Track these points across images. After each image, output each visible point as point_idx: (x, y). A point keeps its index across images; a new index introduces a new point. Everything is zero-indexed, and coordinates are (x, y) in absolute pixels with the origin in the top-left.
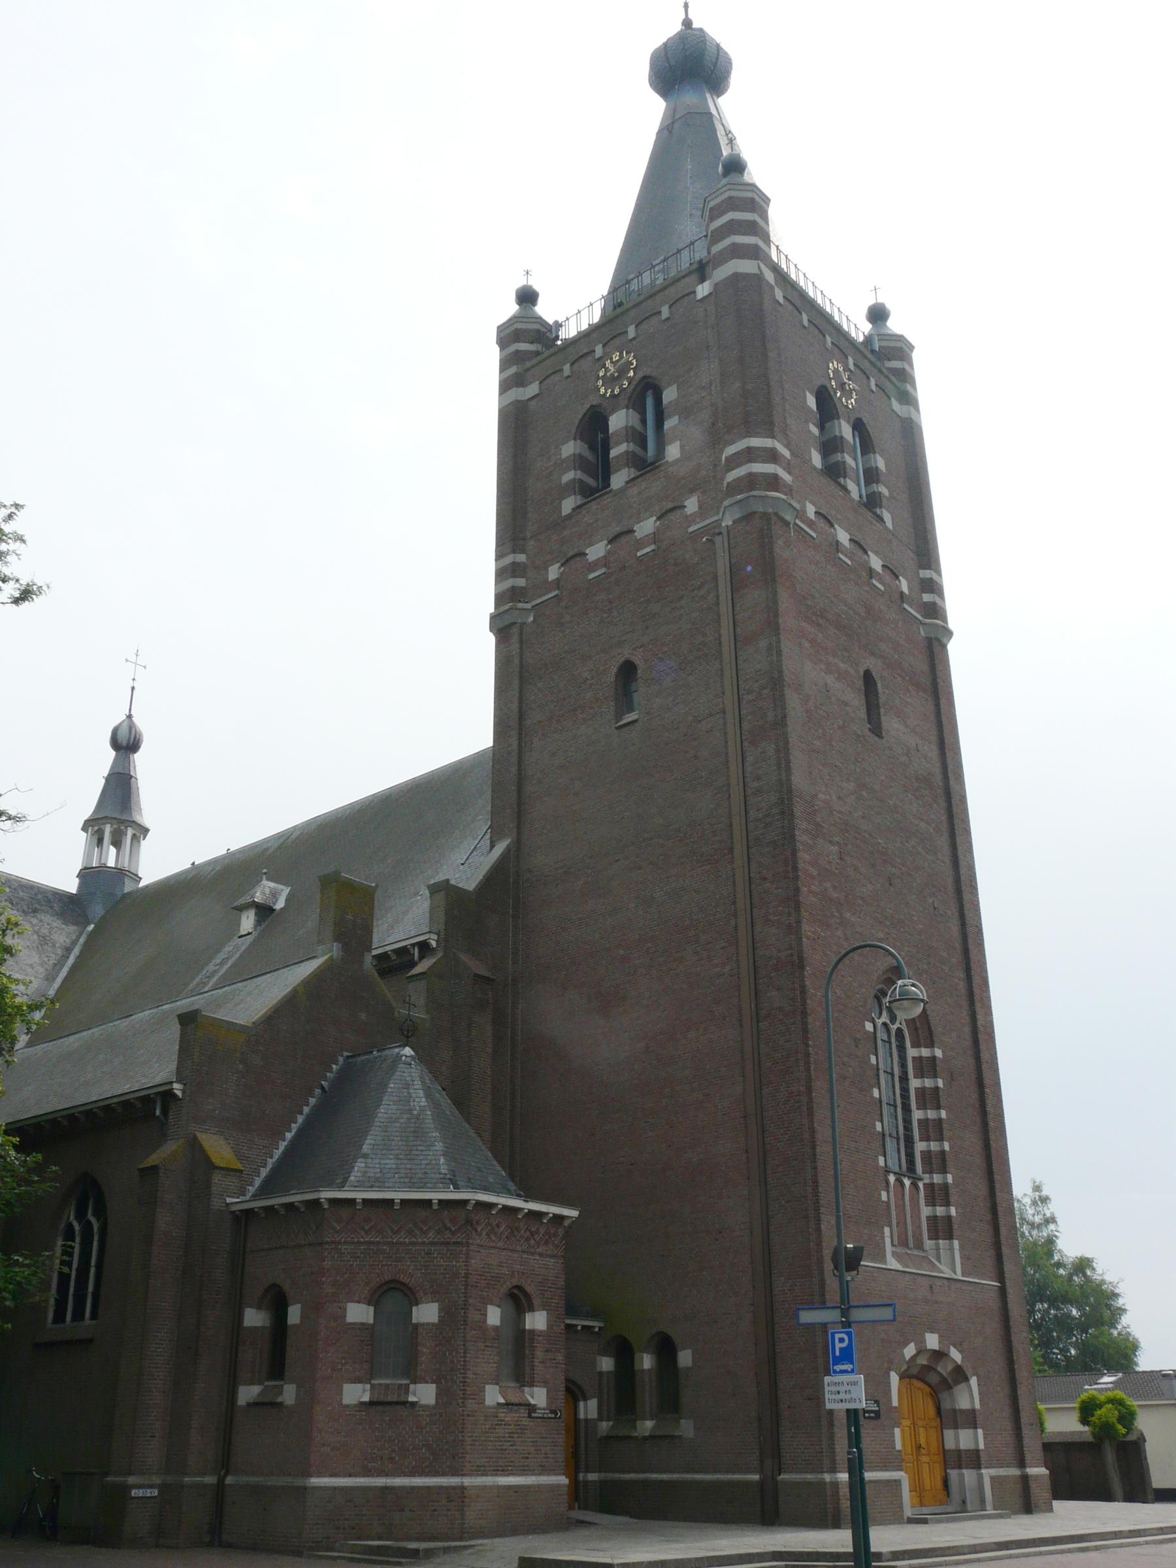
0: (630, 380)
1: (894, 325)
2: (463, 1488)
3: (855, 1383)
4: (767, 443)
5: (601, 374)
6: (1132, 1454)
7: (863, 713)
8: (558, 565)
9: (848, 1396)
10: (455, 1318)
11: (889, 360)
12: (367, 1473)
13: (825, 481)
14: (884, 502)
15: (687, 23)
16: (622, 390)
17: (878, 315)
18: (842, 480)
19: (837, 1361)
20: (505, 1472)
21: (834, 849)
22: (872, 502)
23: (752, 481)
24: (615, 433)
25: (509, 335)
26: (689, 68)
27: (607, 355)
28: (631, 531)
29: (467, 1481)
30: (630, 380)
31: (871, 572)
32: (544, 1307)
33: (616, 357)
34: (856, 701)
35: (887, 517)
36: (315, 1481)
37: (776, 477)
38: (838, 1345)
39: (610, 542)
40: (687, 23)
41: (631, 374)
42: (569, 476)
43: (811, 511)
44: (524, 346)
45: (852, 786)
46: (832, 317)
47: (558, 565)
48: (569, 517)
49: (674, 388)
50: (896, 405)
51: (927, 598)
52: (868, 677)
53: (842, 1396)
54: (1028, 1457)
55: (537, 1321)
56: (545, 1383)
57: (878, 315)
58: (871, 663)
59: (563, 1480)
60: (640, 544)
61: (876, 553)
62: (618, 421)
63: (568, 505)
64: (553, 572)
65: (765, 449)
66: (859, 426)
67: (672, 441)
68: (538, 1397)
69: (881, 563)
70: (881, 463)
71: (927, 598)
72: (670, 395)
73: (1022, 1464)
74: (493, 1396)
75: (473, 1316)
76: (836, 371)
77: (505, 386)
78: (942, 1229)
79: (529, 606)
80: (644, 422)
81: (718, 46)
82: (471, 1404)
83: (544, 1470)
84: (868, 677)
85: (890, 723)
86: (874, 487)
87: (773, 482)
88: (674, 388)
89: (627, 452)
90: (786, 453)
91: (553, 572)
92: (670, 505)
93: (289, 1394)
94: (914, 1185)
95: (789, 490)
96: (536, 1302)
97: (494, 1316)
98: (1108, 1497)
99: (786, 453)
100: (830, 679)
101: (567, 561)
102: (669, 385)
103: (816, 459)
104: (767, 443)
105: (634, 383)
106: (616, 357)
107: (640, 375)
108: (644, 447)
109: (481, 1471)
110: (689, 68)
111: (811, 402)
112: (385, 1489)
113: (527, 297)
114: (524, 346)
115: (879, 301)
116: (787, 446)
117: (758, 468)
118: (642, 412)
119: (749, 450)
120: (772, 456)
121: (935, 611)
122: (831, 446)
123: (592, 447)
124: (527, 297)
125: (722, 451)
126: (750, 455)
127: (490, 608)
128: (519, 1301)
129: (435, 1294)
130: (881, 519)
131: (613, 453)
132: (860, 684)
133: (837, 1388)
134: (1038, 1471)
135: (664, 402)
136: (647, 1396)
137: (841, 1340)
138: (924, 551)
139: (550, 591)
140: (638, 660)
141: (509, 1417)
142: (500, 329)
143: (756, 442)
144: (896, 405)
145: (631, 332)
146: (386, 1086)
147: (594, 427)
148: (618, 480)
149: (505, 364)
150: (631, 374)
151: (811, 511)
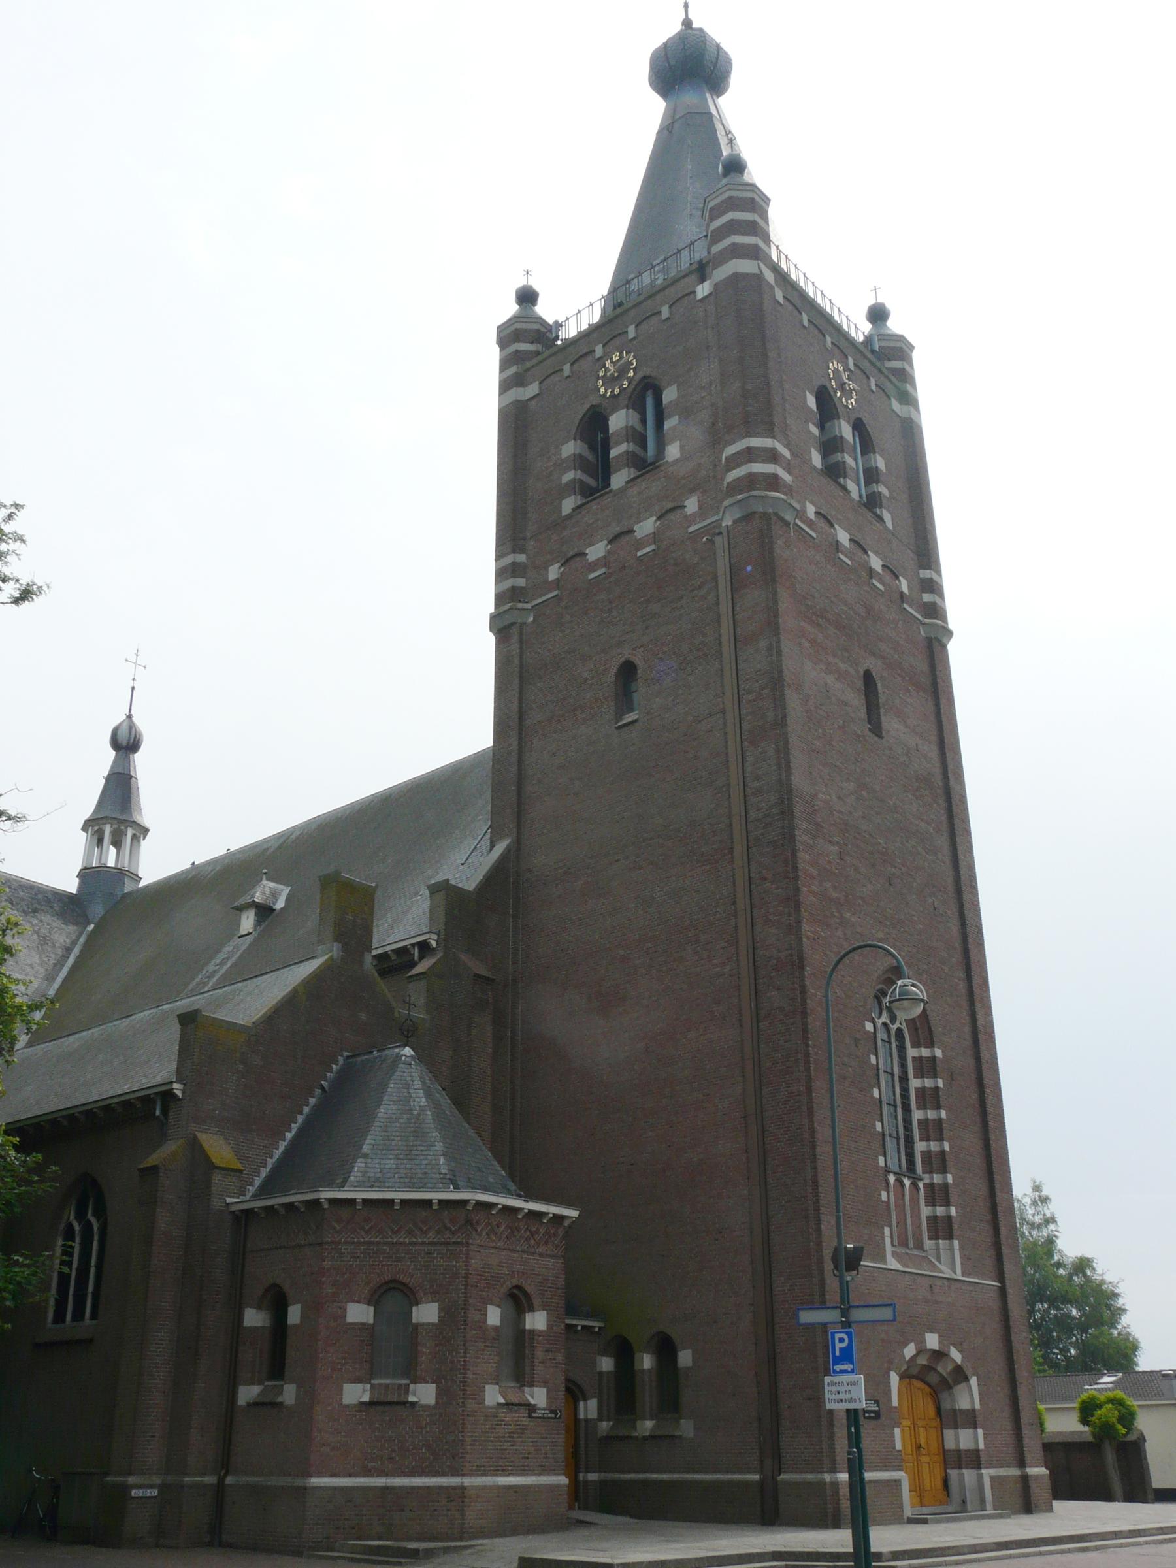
0: (630, 380)
1: (894, 325)
2: (463, 1488)
3: (855, 1383)
4: (767, 443)
5: (601, 374)
6: (1132, 1454)
7: (863, 713)
8: (558, 565)
9: (848, 1396)
10: (455, 1318)
11: (889, 360)
12: (367, 1473)
13: (825, 481)
14: (884, 502)
15: (687, 23)
16: (622, 390)
17: (878, 315)
18: (842, 480)
19: (837, 1361)
20: (505, 1472)
21: (834, 849)
22: (872, 502)
23: (752, 481)
24: (615, 433)
25: (509, 335)
26: (689, 68)
27: (607, 355)
28: (631, 531)
29: (467, 1481)
30: (630, 380)
31: (871, 572)
32: (544, 1307)
33: (616, 357)
34: (856, 701)
35: (887, 517)
36: (315, 1481)
37: (776, 477)
38: (838, 1345)
39: (610, 542)
40: (687, 23)
41: (631, 374)
42: (569, 476)
43: (811, 511)
44: (524, 346)
45: (852, 786)
46: (832, 317)
47: (558, 565)
48: (569, 517)
49: (674, 388)
50: (896, 405)
51: (927, 598)
52: (868, 677)
53: (842, 1396)
54: (1028, 1457)
55: (537, 1321)
56: (545, 1383)
57: (878, 315)
58: (871, 663)
59: (563, 1480)
60: (640, 544)
61: (876, 553)
62: (618, 421)
63: (568, 505)
64: (553, 572)
65: (765, 449)
66: (859, 426)
67: (672, 441)
68: (538, 1397)
69: (881, 563)
70: (881, 463)
71: (927, 598)
72: (670, 395)
73: (1022, 1464)
74: (493, 1396)
75: (473, 1316)
76: (836, 371)
77: (505, 386)
78: (942, 1229)
79: (529, 606)
80: (644, 422)
81: (718, 46)
82: (471, 1404)
83: (544, 1470)
84: (868, 677)
85: (890, 723)
86: (874, 487)
87: (773, 482)
88: (674, 388)
89: (627, 452)
90: (786, 453)
91: (553, 572)
92: (670, 505)
93: (289, 1394)
94: (914, 1185)
95: (789, 490)
96: (536, 1302)
97: (494, 1316)
98: (1108, 1497)
99: (786, 453)
100: (830, 679)
101: (567, 561)
102: (669, 385)
103: (816, 459)
104: (767, 443)
105: (634, 383)
106: (616, 357)
107: (640, 375)
108: (644, 447)
109: (481, 1471)
110: (689, 68)
111: (811, 402)
112: (385, 1489)
113: (527, 297)
114: (524, 346)
115: (879, 301)
116: (787, 446)
117: (758, 468)
118: (642, 412)
119: (749, 450)
120: (772, 456)
121: (935, 611)
122: (831, 446)
123: (592, 447)
124: (527, 297)
125: (722, 451)
126: (750, 455)
127: (490, 608)
128: (519, 1301)
129: (435, 1294)
130: (881, 519)
131: (613, 453)
132: (860, 684)
133: (837, 1388)
134: (1038, 1471)
135: (664, 402)
136: (647, 1396)
137: (841, 1340)
138: (924, 551)
139: (550, 591)
140: (638, 660)
141: (509, 1417)
142: (500, 329)
143: (756, 442)
144: (896, 405)
145: (631, 332)
146: (386, 1086)
147: (594, 427)
148: (618, 480)
149: (505, 364)
150: (631, 374)
151: (811, 511)
